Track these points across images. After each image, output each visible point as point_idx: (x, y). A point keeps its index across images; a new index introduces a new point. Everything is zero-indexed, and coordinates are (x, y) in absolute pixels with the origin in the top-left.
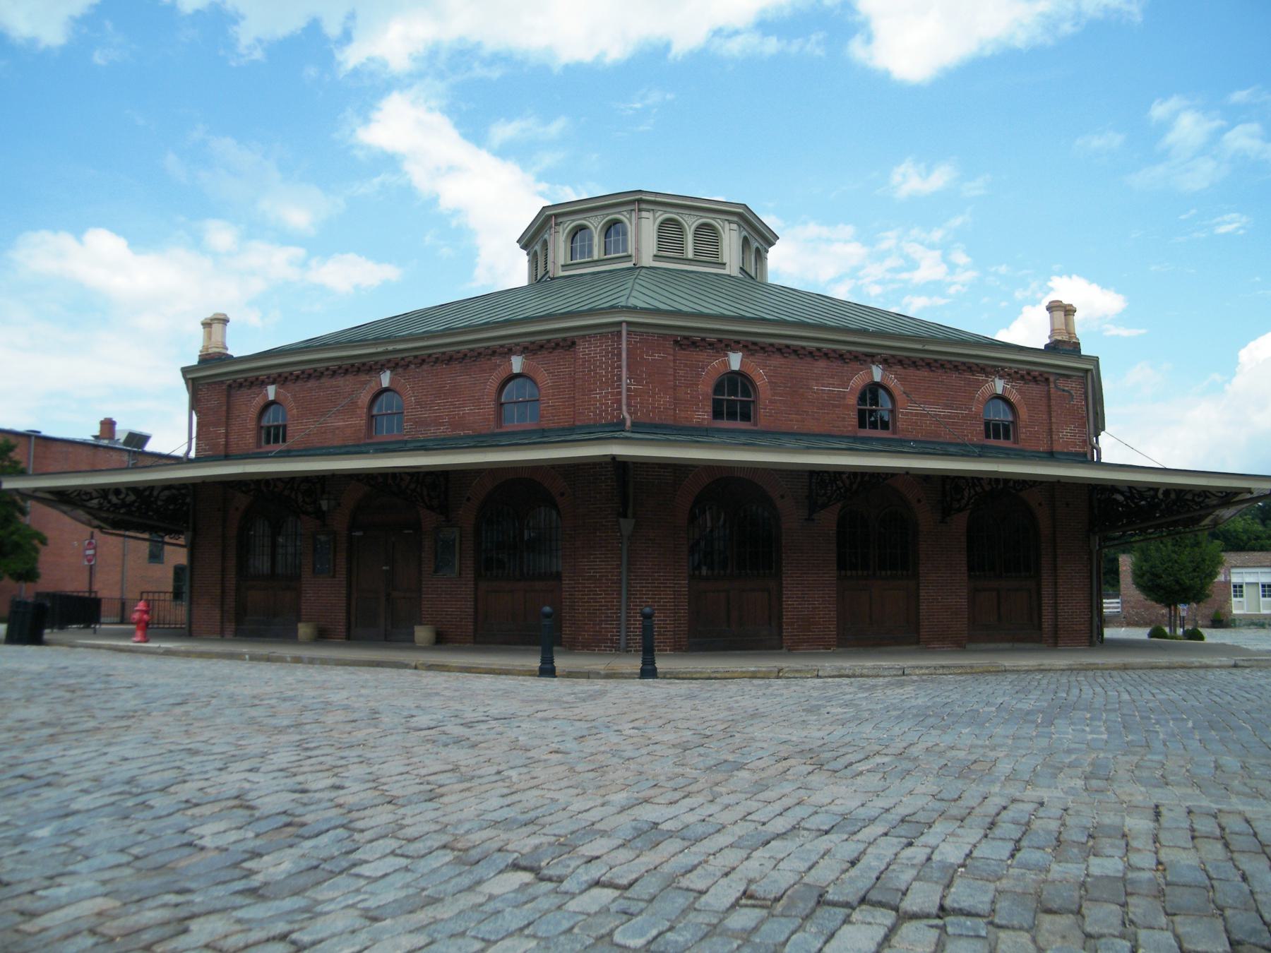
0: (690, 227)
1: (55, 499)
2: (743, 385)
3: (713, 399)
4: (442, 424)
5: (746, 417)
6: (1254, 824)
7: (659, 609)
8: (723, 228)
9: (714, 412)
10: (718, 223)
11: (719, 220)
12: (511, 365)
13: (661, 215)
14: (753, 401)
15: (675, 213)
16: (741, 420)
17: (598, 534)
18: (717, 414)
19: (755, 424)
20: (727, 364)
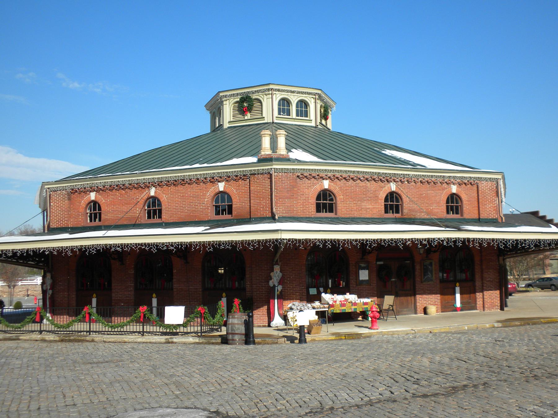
0: (294, 102)
1: (208, 227)
2: (396, 198)
3: (385, 204)
4: (422, 212)
5: (331, 211)
6: (299, 403)
7: (287, 284)
8: (311, 102)
9: (385, 211)
10: (307, 98)
11: (308, 98)
12: (451, 189)
13: (279, 96)
14: (335, 203)
15: (304, 97)
16: (329, 212)
17: (491, 263)
18: (318, 210)
19: (336, 214)
20: (322, 185)
